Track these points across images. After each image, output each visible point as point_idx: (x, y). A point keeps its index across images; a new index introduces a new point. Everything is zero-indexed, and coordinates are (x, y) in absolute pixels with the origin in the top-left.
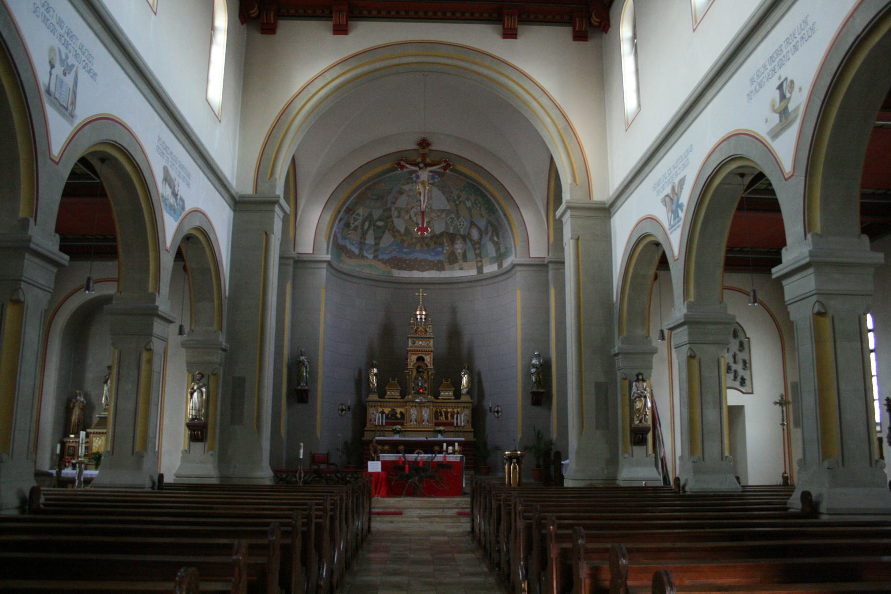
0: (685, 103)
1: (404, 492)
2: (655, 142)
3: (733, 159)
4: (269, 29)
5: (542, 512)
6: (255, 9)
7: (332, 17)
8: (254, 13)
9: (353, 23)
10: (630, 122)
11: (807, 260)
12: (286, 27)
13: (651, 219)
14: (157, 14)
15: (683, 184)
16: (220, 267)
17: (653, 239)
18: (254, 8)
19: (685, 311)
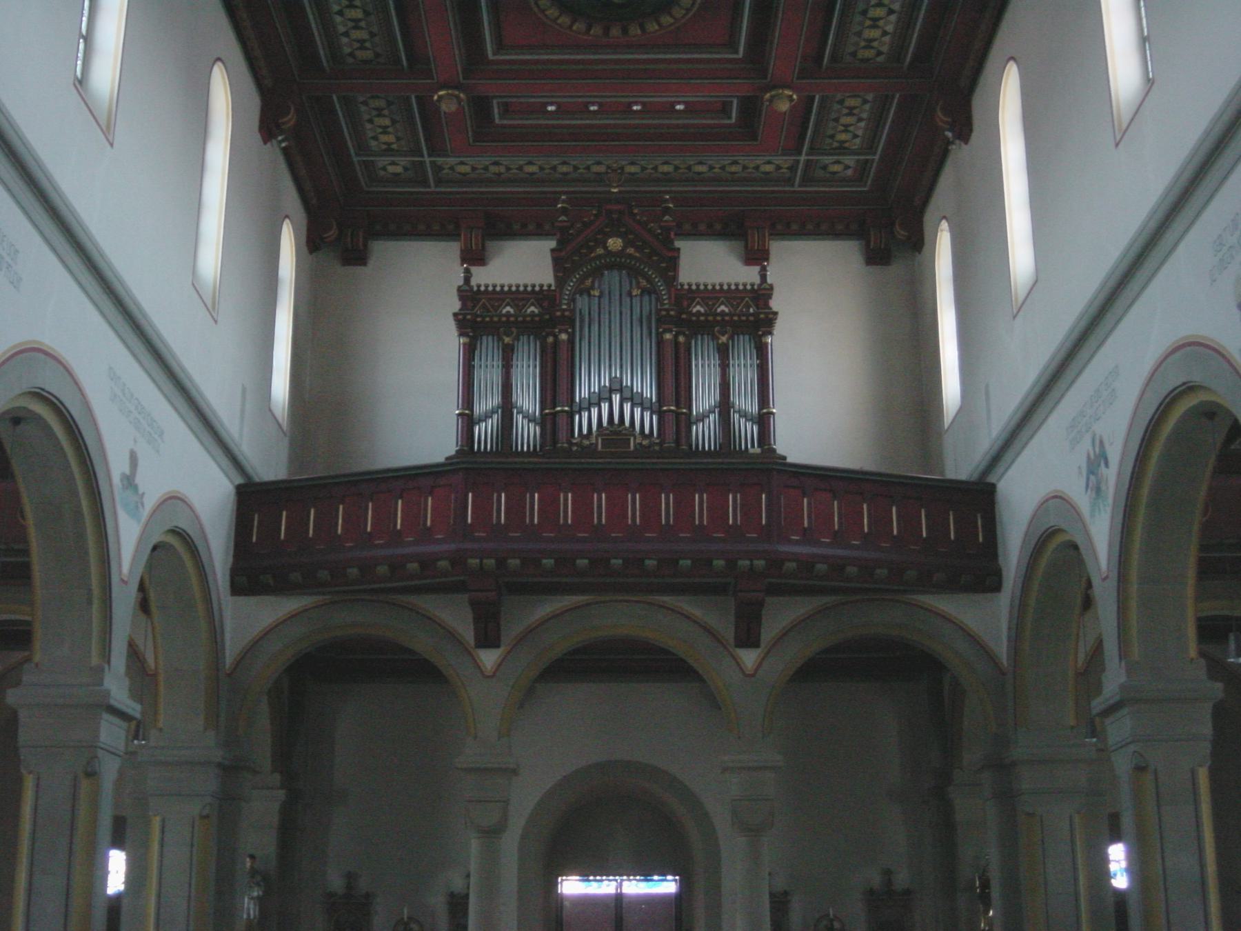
0: (1072, 330)
1: (463, 330)
2: (1053, 358)
3: (1189, 389)
4: (356, 257)
5: (163, 821)
6: (290, 116)
7: (459, 235)
8: (332, 235)
9: (495, 243)
10: (1124, 126)
11: (1117, 698)
12: (385, 251)
13: (1058, 497)
14: (114, 146)
15: (720, 860)
16: (210, 578)
17: (1067, 538)
18: (289, 113)
19: (1123, 679)
